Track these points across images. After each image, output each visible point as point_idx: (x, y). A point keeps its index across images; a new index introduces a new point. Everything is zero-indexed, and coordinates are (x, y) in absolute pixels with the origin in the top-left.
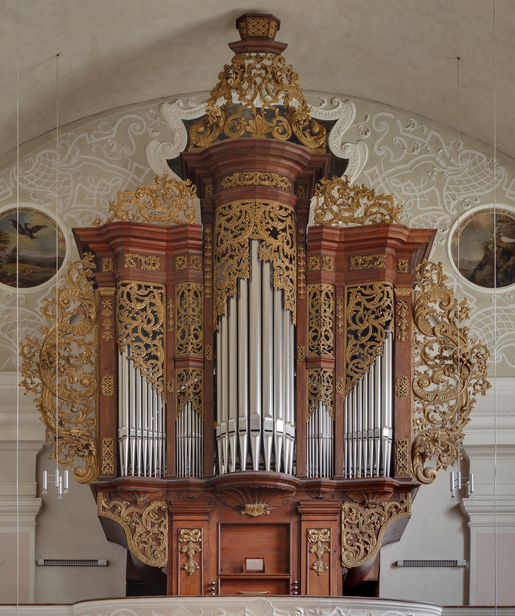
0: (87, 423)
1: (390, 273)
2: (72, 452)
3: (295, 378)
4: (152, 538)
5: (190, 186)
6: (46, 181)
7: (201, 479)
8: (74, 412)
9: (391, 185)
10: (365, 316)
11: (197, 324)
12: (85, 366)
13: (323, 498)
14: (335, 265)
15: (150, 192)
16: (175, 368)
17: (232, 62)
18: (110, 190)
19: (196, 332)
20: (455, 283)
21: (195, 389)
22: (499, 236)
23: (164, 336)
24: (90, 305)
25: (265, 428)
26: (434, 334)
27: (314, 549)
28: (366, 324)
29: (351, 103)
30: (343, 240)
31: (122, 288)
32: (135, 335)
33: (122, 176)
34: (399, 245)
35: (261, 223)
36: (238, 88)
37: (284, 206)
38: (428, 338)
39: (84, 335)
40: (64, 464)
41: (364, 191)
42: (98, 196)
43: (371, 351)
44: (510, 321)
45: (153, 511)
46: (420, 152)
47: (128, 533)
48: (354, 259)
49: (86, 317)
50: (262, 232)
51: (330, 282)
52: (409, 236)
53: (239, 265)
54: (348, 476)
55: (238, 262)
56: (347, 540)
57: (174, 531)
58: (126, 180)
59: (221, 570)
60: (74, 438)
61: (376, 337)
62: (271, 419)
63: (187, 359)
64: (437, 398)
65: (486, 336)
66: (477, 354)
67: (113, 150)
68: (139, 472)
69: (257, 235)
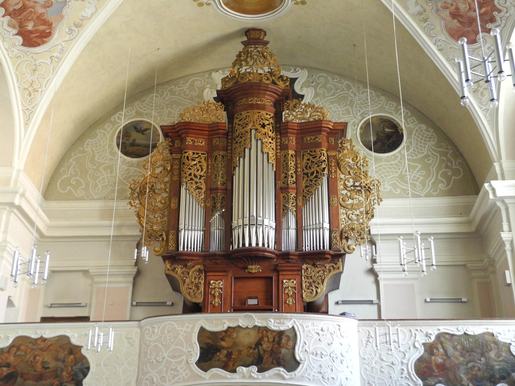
8: (155, 217)
21: (221, 204)
24: (168, 163)
26: (350, 174)
29: (305, 70)
30: (299, 128)
31: (184, 154)
36: (245, 60)
37: (269, 113)
38: (346, 176)
39: (164, 178)
41: (309, 106)
43: (315, 183)
45: (195, 270)
47: (181, 283)
50: (257, 126)
56: (306, 286)
57: (207, 282)
59: (234, 304)
62: (262, 219)
65: (381, 177)
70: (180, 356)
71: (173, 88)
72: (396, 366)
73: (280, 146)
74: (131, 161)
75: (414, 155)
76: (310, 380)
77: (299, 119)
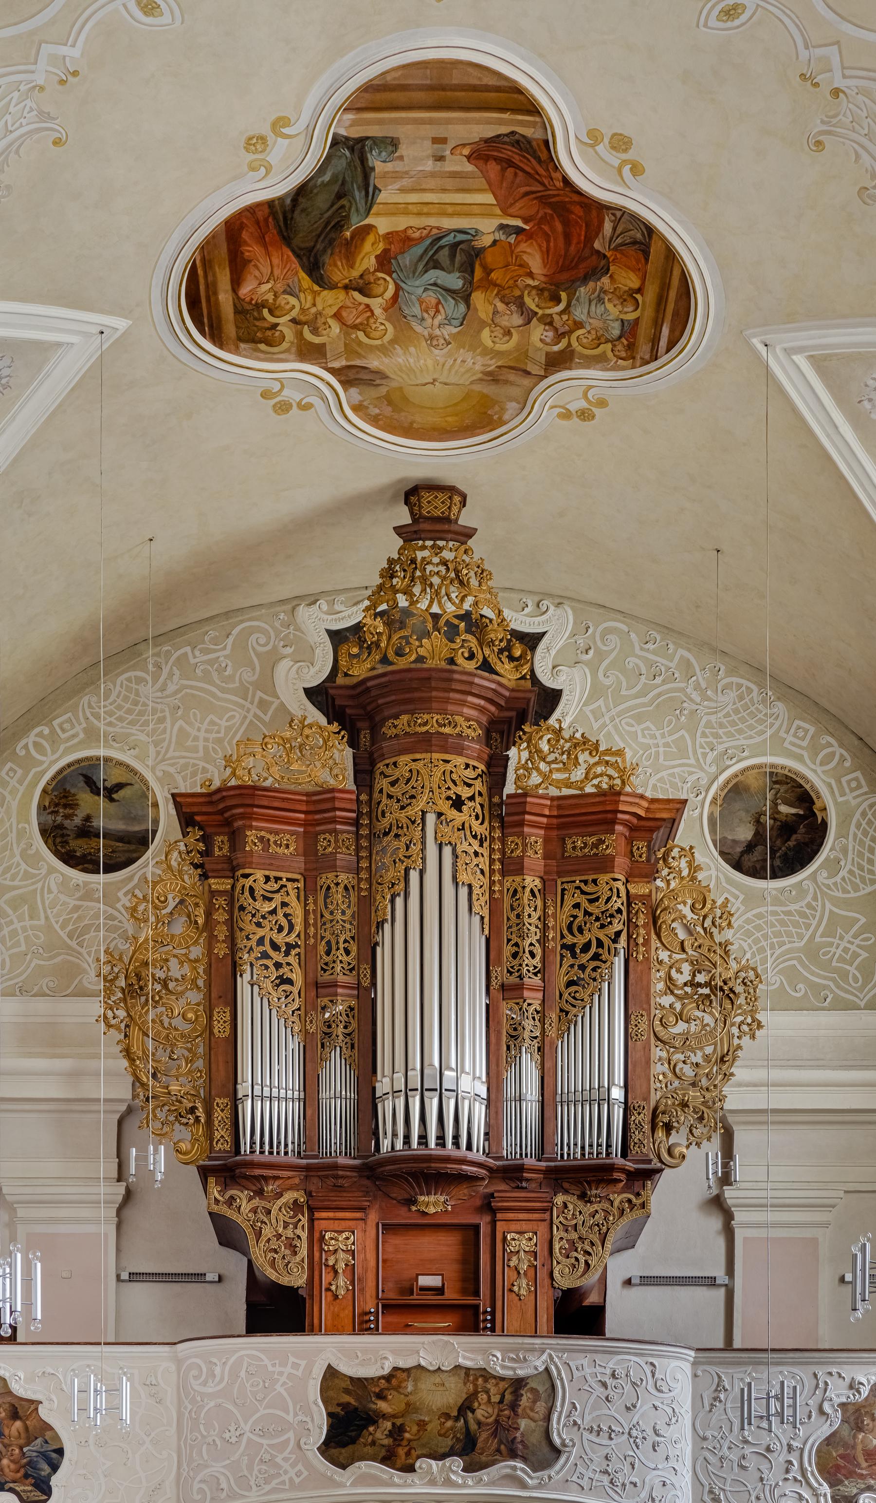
0: (193, 1076)
1: (621, 862)
2: (172, 1118)
3: (487, 1006)
4: (285, 1245)
5: (339, 733)
6: (131, 718)
7: (355, 1158)
8: (174, 1060)
9: (623, 728)
10: (585, 924)
11: (348, 933)
12: (189, 994)
13: (526, 1188)
14: (544, 848)
15: (281, 742)
16: (317, 997)
17: (399, 554)
18: (223, 731)
19: (346, 945)
20: (713, 873)
21: (345, 1027)
22: (775, 805)
23: (302, 950)
24: (197, 905)
25: (445, 1086)
26: (683, 950)
27: (514, 1262)
28: (587, 936)
29: (566, 607)
30: (555, 813)
31: (242, 880)
32: (261, 948)
33: (241, 711)
34: (635, 821)
35: (440, 788)
36: (407, 592)
37: (472, 763)
38: (674, 955)
39: (187, 948)
40: (160, 1136)
42: (206, 740)
43: (594, 975)
44: (791, 928)
45: (285, 1205)
46: (664, 681)
48: (570, 841)
49: (191, 922)
50: (441, 802)
51: (537, 874)
52: (647, 808)
53: (407, 850)
54: (562, 1155)
55: (406, 844)
56: (561, 1248)
57: (317, 1235)
58: (245, 717)
59: (383, 1291)
60: (174, 1098)
61: (601, 955)
62: (454, 1074)
63: (335, 985)
64: (688, 1043)
66: (744, 979)
67: (227, 673)
68: (267, 1148)
69: (434, 807)
70: (283, 1431)
71: (186, 654)
72: (775, 1454)
73: (502, 862)
74: (86, 884)
75: (849, 888)
76: (583, 1489)
77: (558, 784)
